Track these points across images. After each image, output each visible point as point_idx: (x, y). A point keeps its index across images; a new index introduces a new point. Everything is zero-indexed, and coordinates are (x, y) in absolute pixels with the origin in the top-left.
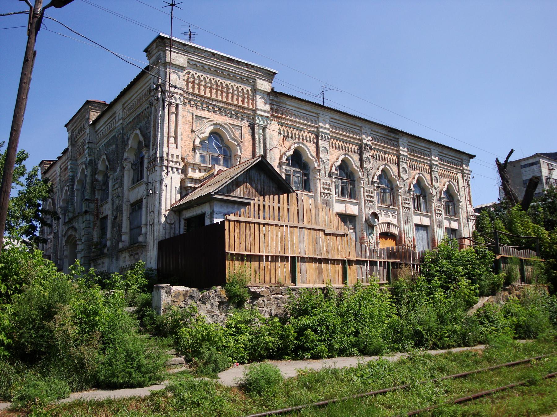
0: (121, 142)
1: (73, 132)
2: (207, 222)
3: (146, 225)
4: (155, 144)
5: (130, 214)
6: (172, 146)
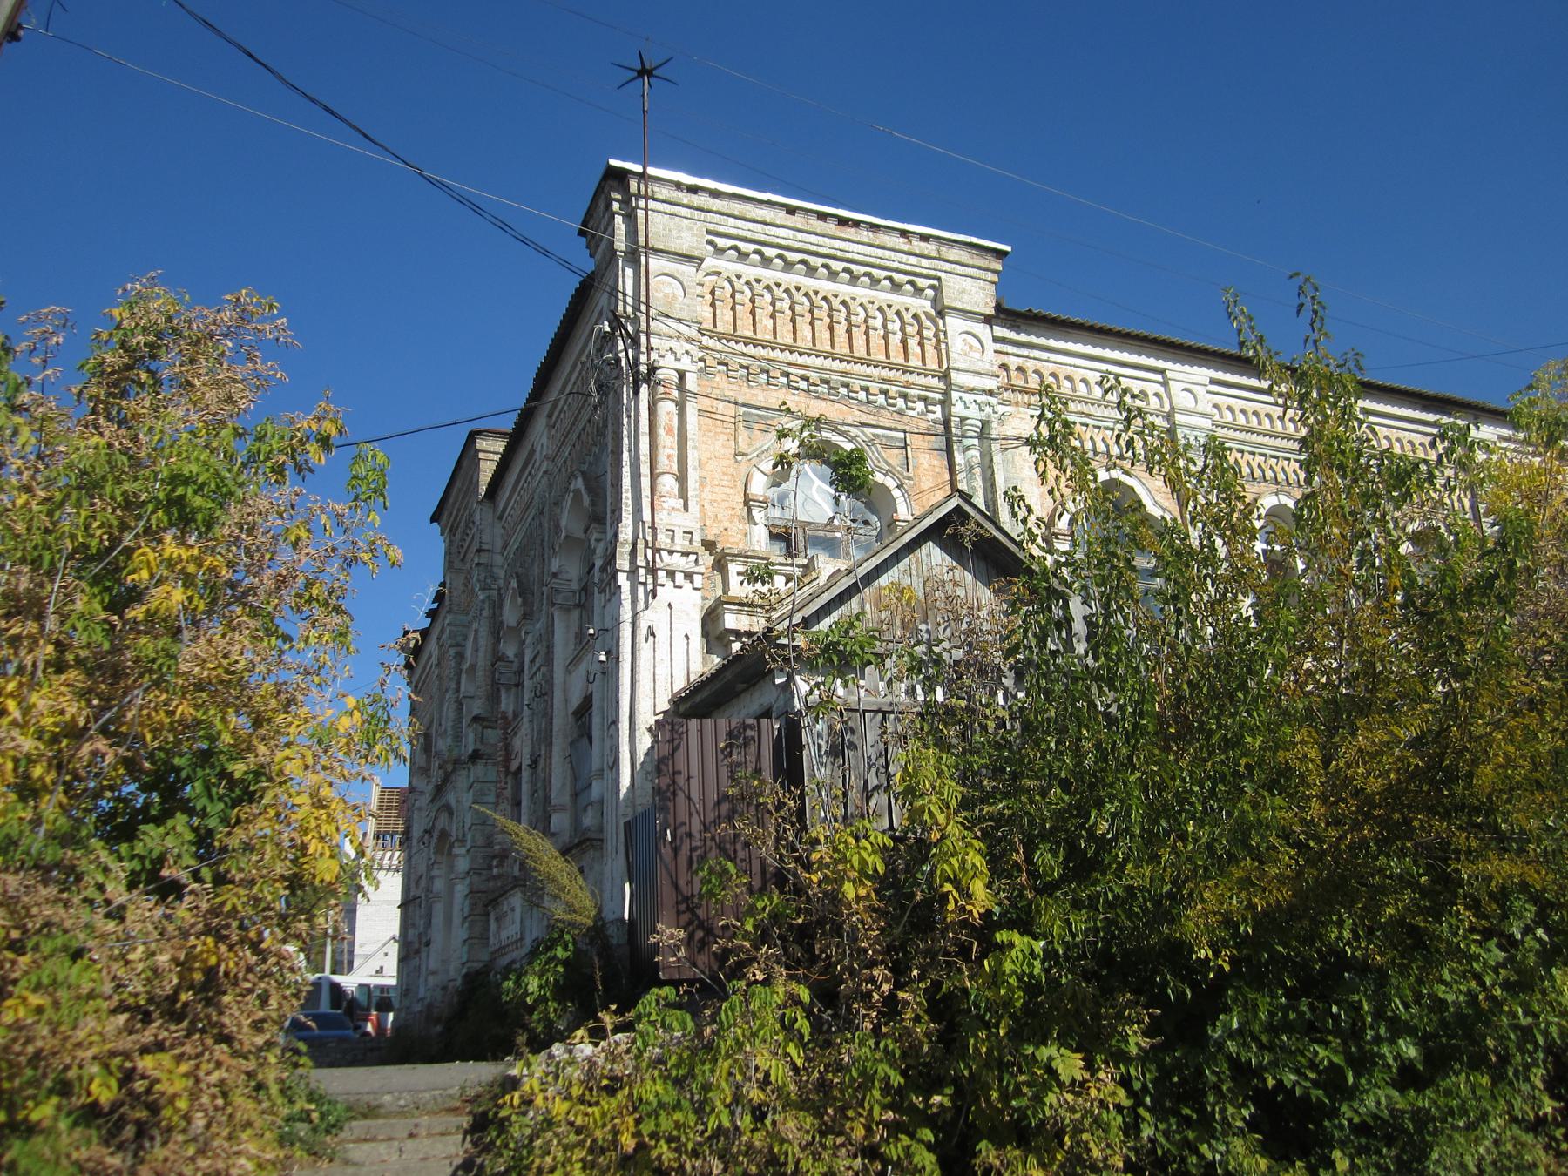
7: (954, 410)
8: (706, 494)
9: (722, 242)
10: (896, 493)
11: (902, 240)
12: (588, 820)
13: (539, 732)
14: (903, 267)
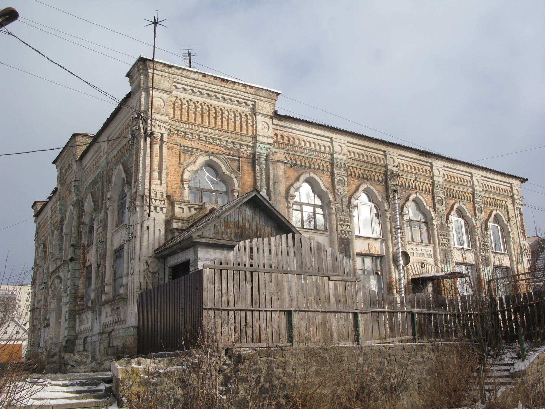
0: (104, 179)
1: (61, 169)
2: (191, 269)
3: (128, 274)
4: (136, 181)
5: (114, 261)
6: (156, 181)
7: (257, 150)
8: (169, 178)
9: (179, 86)
10: (235, 180)
11: (243, 88)
12: (122, 291)
13: (100, 255)
14: (243, 97)
